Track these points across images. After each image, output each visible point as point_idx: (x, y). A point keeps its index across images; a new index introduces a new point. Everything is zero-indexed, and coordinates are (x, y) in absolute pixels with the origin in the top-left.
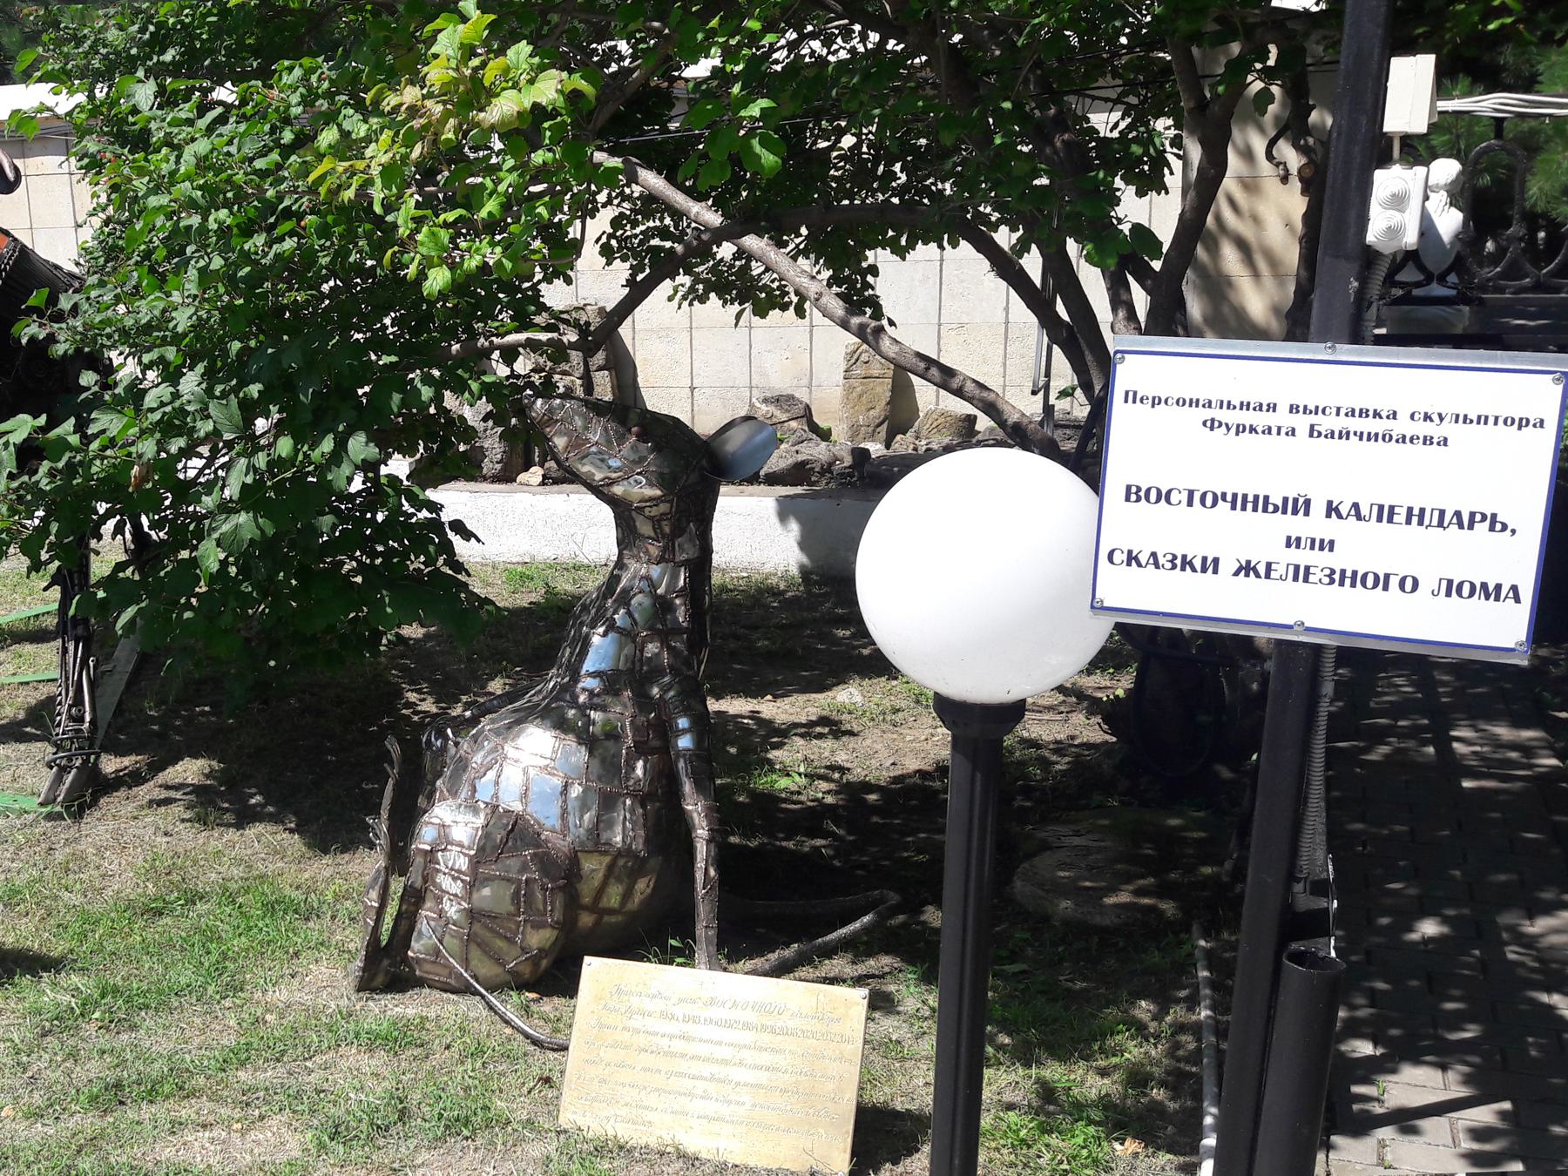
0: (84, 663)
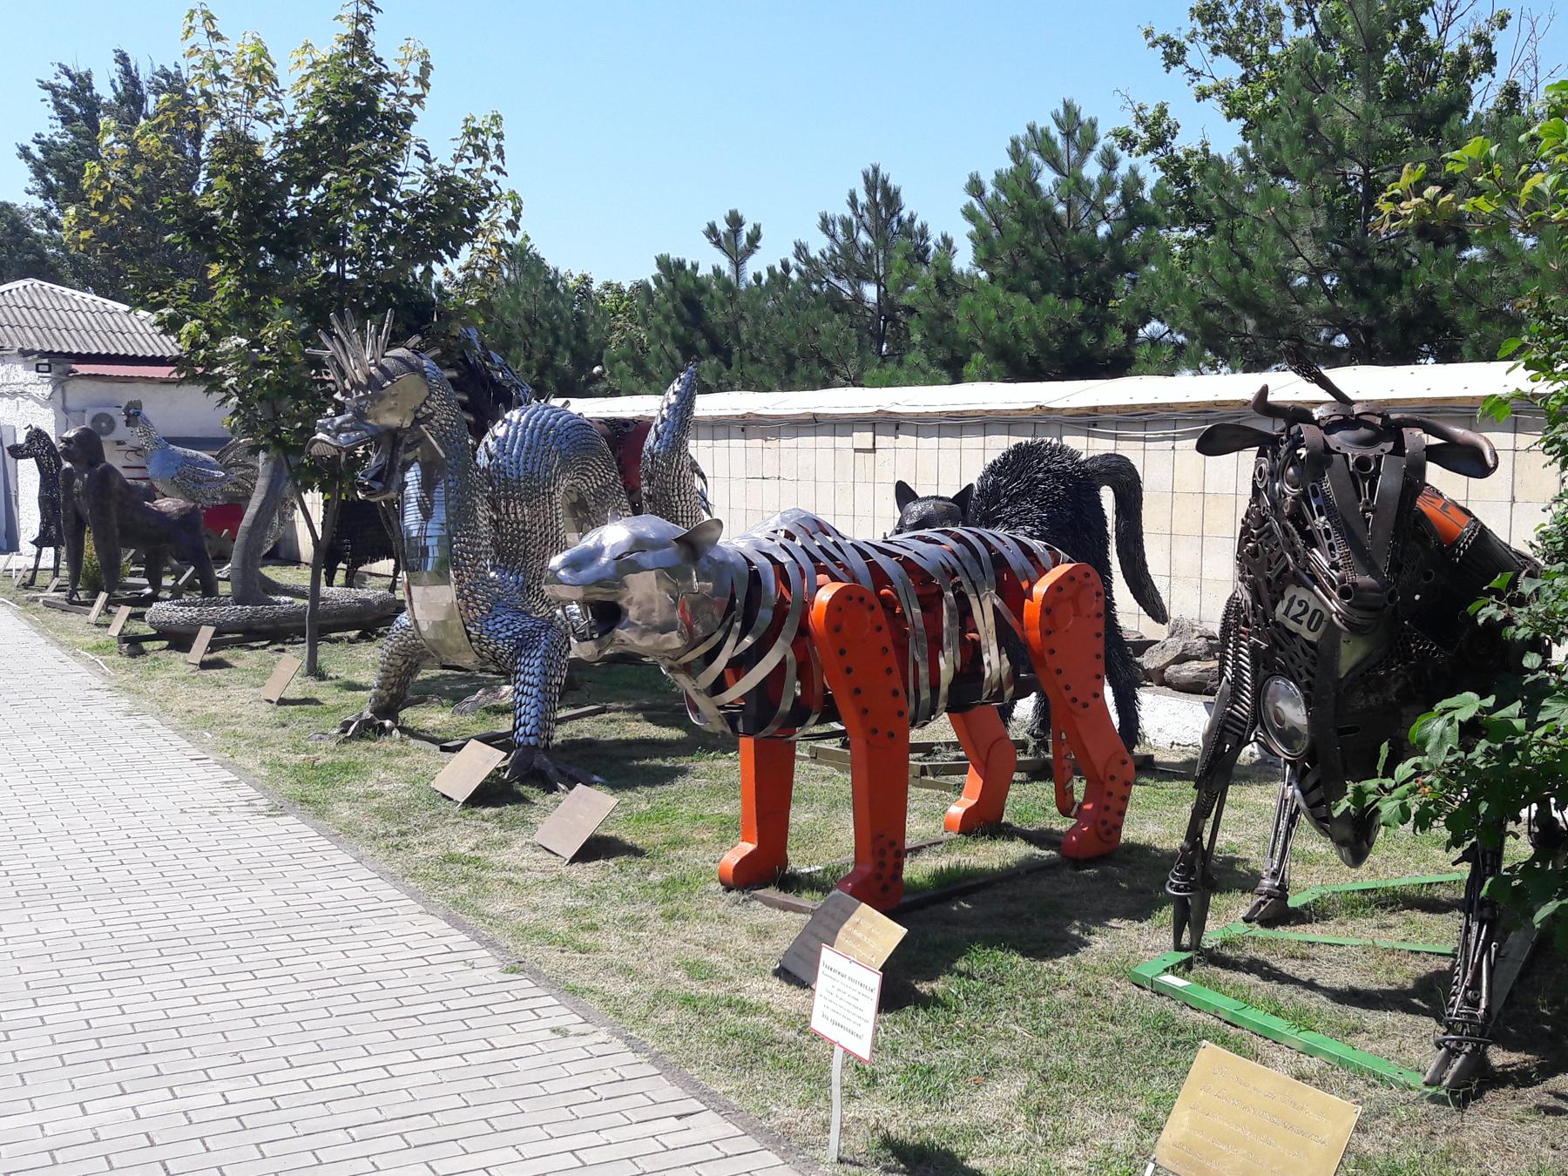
0: (1486, 947)
